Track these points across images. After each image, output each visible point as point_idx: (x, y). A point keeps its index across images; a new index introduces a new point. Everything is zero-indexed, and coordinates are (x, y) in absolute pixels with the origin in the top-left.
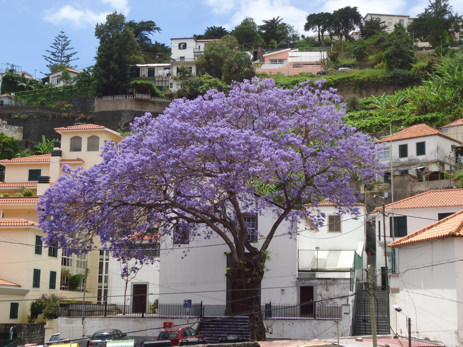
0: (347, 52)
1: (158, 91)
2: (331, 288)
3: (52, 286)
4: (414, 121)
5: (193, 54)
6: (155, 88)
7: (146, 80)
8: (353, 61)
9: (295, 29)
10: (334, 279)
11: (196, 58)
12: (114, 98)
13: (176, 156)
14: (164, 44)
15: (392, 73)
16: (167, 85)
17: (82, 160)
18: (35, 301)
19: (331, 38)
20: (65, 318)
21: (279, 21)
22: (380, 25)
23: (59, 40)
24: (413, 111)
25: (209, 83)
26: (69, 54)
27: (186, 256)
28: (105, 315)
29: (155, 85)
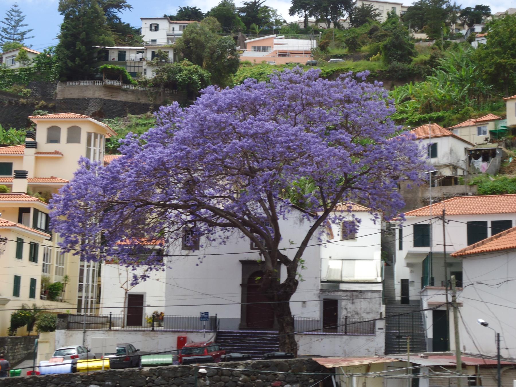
0: (338, 42)
1: (130, 77)
2: (357, 301)
3: (32, 295)
4: (419, 120)
5: (166, 37)
6: (127, 74)
7: (117, 64)
8: (345, 51)
9: (278, 13)
10: (361, 291)
11: (170, 42)
12: (79, 84)
13: (215, 151)
14: (129, 24)
15: (390, 66)
16: (140, 71)
17: (60, 154)
18: (16, 312)
19: (316, 24)
20: (63, 331)
21: (261, 3)
22: (372, 12)
23: (12, 15)
24: (416, 109)
25: (189, 71)
26: (23, 31)
27: (201, 262)
28: (110, 328)
29: (127, 70)
